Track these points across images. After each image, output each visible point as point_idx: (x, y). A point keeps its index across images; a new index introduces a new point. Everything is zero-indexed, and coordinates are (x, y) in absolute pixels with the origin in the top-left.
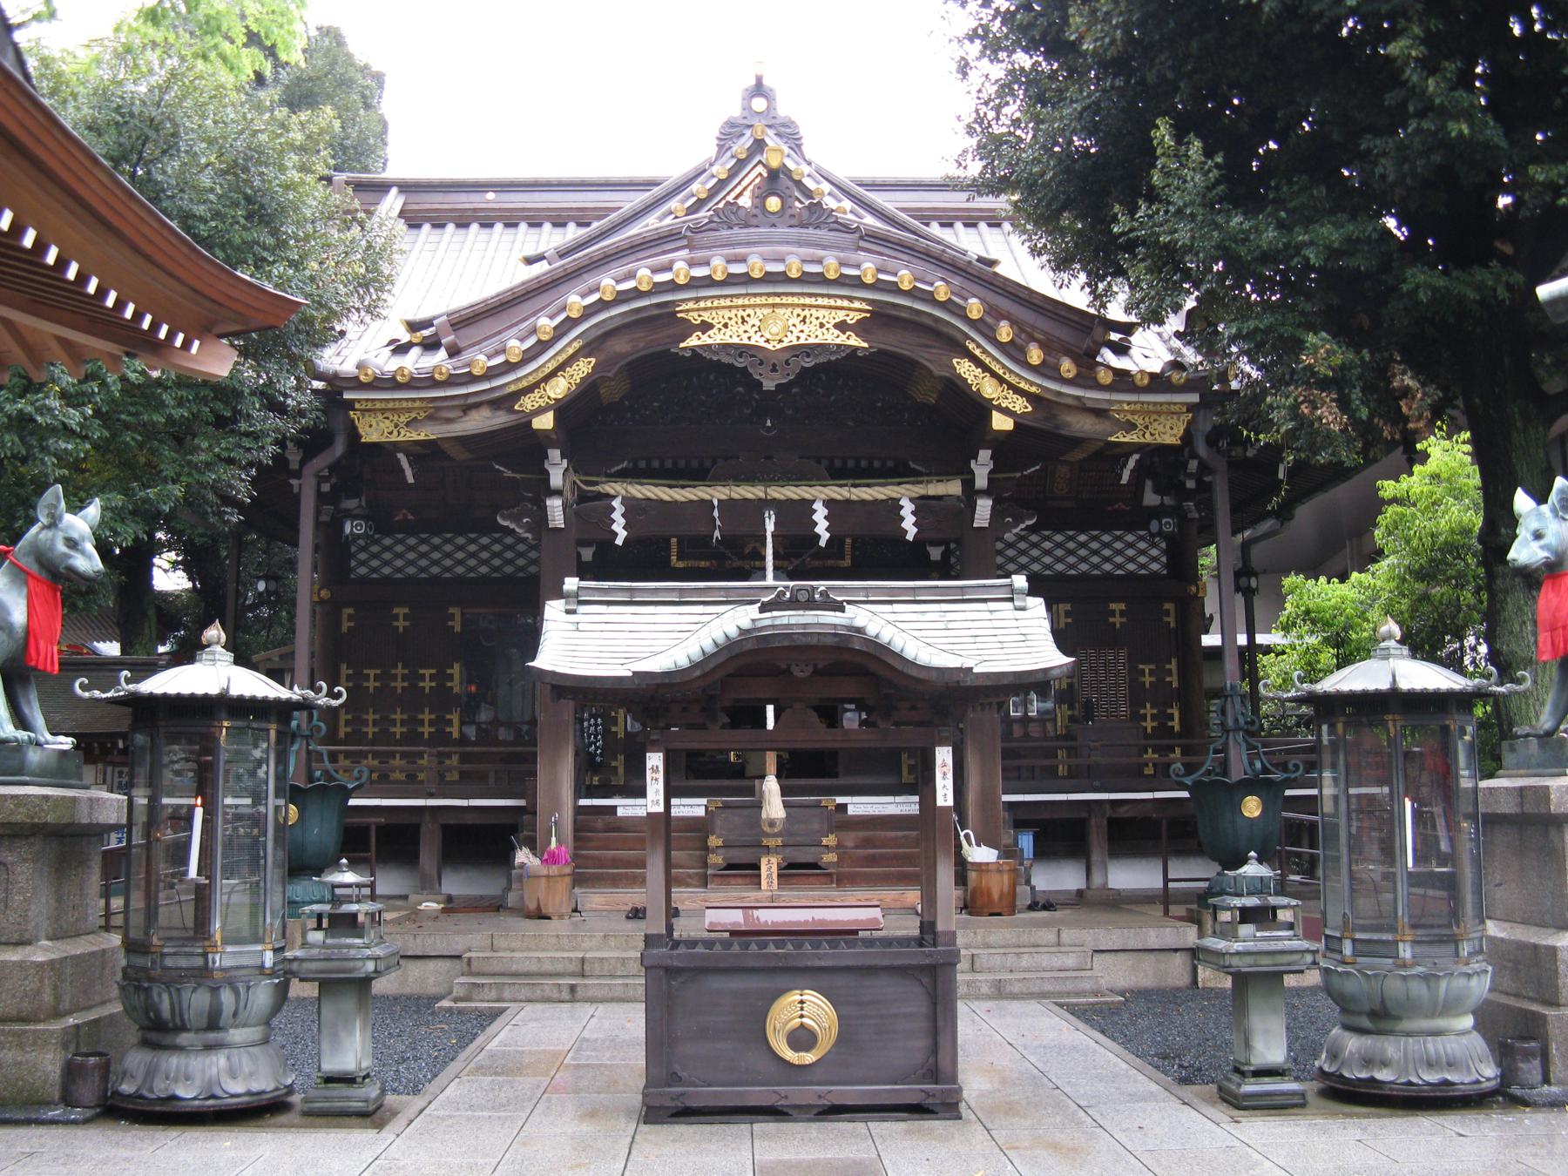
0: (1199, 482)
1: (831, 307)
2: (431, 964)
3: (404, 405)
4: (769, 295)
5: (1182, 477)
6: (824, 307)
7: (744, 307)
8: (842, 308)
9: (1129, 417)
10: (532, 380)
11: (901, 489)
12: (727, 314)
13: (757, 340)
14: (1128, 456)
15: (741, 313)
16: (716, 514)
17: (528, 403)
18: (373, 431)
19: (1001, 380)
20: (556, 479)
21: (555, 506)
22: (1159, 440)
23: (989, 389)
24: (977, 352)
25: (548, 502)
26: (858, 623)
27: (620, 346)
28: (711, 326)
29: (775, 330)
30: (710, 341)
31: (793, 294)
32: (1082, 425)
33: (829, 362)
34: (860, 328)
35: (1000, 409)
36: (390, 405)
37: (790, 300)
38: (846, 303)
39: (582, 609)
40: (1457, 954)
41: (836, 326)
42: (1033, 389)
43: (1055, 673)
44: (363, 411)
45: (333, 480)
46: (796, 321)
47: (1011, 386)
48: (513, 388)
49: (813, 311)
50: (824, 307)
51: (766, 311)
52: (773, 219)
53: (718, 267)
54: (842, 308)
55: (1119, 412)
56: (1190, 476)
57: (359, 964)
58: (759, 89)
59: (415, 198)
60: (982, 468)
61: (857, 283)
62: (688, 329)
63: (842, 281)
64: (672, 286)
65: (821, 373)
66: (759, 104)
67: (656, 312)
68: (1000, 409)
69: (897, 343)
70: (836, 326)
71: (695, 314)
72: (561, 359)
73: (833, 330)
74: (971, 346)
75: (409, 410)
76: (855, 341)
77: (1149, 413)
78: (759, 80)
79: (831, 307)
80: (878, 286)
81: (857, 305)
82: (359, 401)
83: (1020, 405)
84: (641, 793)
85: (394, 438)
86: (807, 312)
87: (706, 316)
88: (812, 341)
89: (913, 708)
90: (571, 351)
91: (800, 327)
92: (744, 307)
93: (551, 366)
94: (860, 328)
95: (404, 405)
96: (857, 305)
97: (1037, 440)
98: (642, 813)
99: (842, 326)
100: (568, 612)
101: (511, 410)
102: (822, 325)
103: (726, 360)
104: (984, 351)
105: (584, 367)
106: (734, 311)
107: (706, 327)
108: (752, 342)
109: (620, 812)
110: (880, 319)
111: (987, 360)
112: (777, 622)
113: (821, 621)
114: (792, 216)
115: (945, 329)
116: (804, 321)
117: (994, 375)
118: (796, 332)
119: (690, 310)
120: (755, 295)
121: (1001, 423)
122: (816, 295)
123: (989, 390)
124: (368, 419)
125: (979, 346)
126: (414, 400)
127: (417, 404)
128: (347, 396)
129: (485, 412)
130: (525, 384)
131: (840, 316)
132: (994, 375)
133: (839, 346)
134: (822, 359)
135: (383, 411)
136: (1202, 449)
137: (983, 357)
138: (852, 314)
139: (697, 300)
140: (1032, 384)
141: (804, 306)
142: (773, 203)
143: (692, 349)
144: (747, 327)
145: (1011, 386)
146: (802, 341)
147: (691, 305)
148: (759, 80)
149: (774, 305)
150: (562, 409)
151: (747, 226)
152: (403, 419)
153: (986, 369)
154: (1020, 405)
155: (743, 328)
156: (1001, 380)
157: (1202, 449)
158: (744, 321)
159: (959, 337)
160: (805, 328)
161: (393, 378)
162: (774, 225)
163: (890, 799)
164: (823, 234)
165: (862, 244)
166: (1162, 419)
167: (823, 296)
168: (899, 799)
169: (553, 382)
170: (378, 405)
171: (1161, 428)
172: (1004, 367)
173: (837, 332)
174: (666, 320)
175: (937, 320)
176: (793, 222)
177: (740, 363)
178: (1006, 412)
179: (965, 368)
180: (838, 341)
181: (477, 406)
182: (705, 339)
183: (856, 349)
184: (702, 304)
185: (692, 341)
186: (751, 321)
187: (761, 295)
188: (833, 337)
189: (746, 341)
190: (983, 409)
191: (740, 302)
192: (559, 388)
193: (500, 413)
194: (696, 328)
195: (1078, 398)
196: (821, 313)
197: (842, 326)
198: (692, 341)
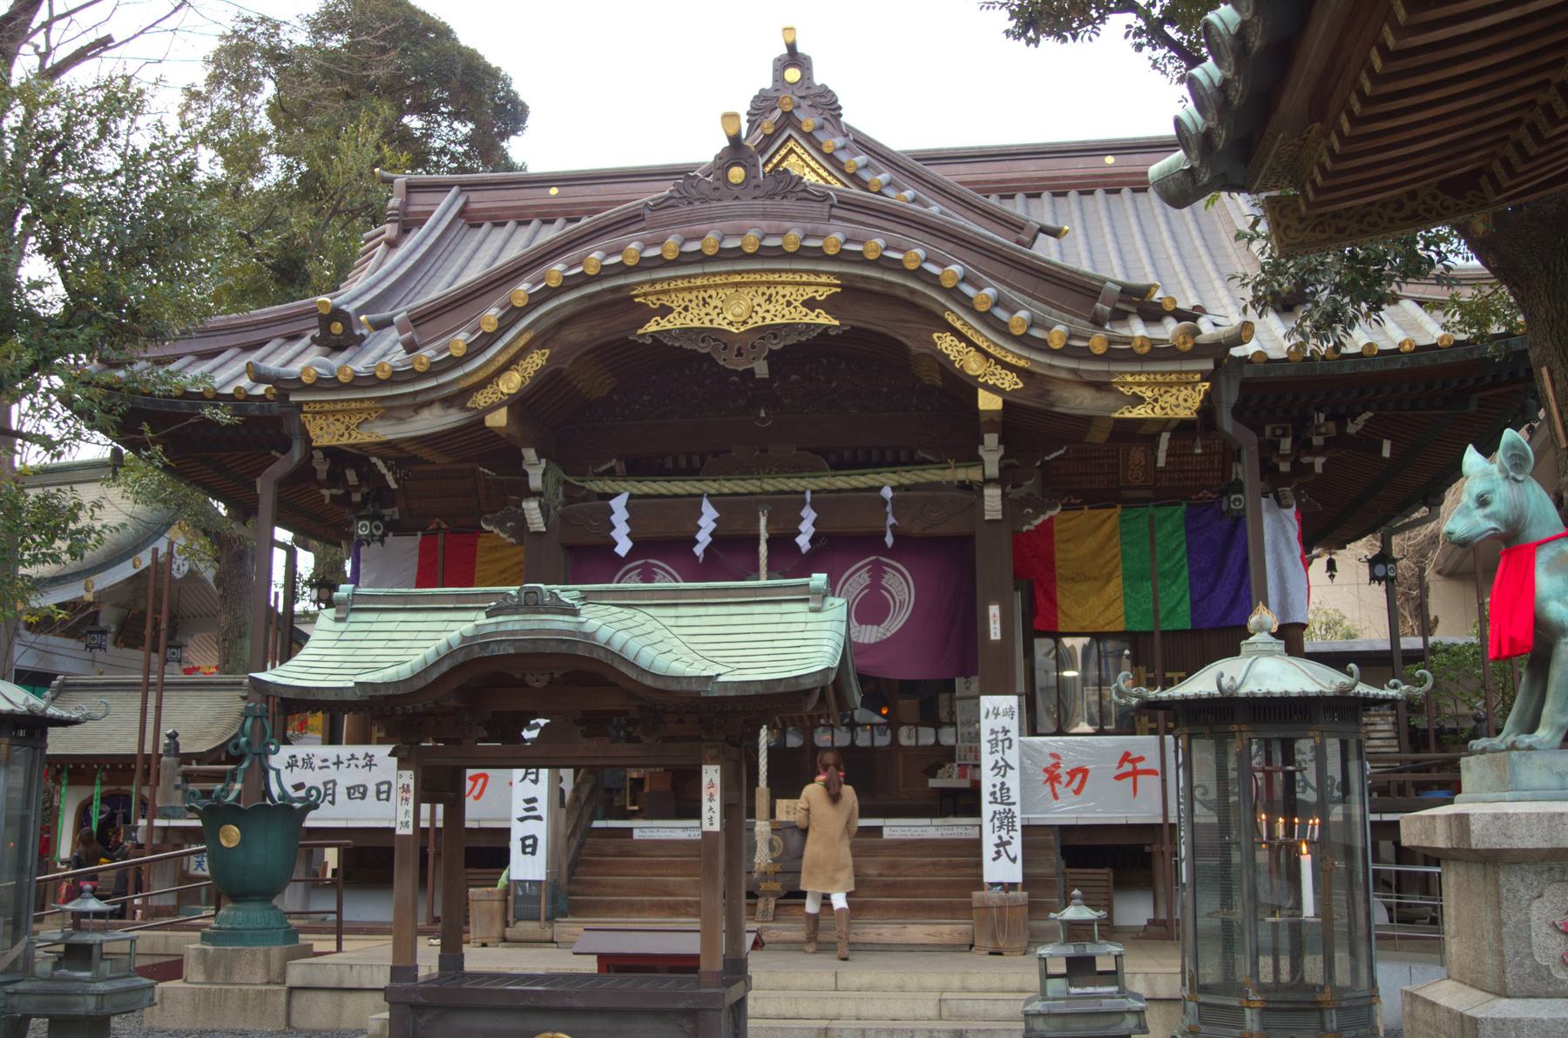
0: (1296, 464)
1: (798, 284)
2: (367, 995)
3: (353, 405)
4: (729, 273)
5: (1275, 460)
6: (790, 283)
7: (705, 288)
8: (810, 284)
9: (1136, 389)
10: (481, 375)
11: (804, 483)
12: (688, 296)
13: (720, 323)
14: (1158, 435)
15: (702, 294)
16: (889, 508)
17: (481, 399)
18: (325, 433)
19: (987, 355)
20: (535, 482)
21: (531, 508)
22: (1171, 414)
23: (973, 365)
24: (958, 325)
25: (524, 505)
26: (588, 628)
27: (576, 335)
28: (671, 310)
29: (738, 310)
30: (669, 326)
31: (754, 271)
32: (1081, 401)
33: (800, 343)
34: (830, 305)
35: (986, 386)
36: (339, 406)
37: (752, 277)
38: (812, 279)
39: (352, 617)
40: (1323, 1027)
41: (804, 304)
42: (1022, 363)
43: (808, 684)
44: (315, 413)
45: (365, 490)
46: (760, 300)
47: (998, 361)
48: (463, 384)
49: (779, 288)
50: (790, 283)
51: (729, 291)
52: (736, 191)
53: (672, 245)
54: (810, 284)
55: (1124, 384)
56: (1284, 457)
57: (81, 999)
58: (793, 57)
59: (474, 196)
60: (991, 451)
61: (819, 255)
62: (647, 314)
63: (802, 254)
64: (623, 269)
65: (796, 354)
66: (793, 75)
67: (610, 297)
68: (986, 386)
69: (873, 318)
70: (804, 304)
71: (653, 298)
72: (512, 351)
73: (801, 308)
74: (950, 318)
75: (360, 411)
76: (825, 319)
77: (1158, 384)
78: (792, 47)
79: (798, 284)
80: (842, 257)
81: (824, 279)
82: (307, 403)
83: (1009, 381)
84: (696, 813)
85: (344, 441)
86: (772, 290)
87: (665, 300)
88: (778, 321)
89: (681, 721)
90: (522, 343)
91: (766, 306)
92: (705, 288)
93: (502, 359)
94: (830, 305)
95: (353, 405)
96: (824, 279)
97: (1027, 424)
98: (696, 835)
99: (810, 304)
100: (337, 620)
101: (463, 408)
102: (789, 304)
103: (688, 346)
104: (965, 324)
105: (537, 360)
106: (695, 293)
107: (665, 311)
108: (715, 325)
109: (637, 835)
110: (850, 294)
111: (969, 334)
112: (502, 628)
113: (548, 626)
114: (757, 186)
115: (921, 301)
116: (769, 300)
117: (979, 349)
118: (761, 314)
119: (644, 290)
120: (714, 274)
121: (988, 402)
122: (780, 271)
123: (974, 366)
124: (321, 421)
125: (959, 318)
126: (362, 400)
127: (365, 405)
128: (292, 399)
129: (437, 410)
130: (475, 379)
131: (809, 292)
132: (979, 349)
133: (808, 325)
134: (792, 341)
135: (333, 413)
136: (1227, 423)
137: (964, 330)
138: (821, 290)
139: (653, 282)
140: (1020, 357)
141: (769, 284)
142: (737, 174)
143: (653, 335)
144: (709, 309)
145: (998, 361)
146: (768, 322)
147: (646, 288)
148: (792, 47)
149: (737, 285)
150: (519, 404)
151: (704, 200)
152: (354, 421)
153: (970, 343)
154: (1009, 381)
155: (704, 310)
156: (987, 355)
157: (1227, 423)
158: (705, 303)
159: (938, 310)
160: (771, 307)
161: (299, 379)
162: (737, 198)
163: (927, 821)
164: (789, 204)
165: (835, 211)
166: (1174, 390)
167: (786, 271)
168: (936, 821)
169: (506, 376)
170: (327, 407)
171: (1172, 400)
172: (988, 340)
173: (805, 310)
174: (622, 305)
175: (912, 291)
176: (757, 193)
177: (703, 349)
178: (994, 389)
179: (946, 343)
180: (806, 320)
181: (429, 404)
182: (665, 324)
183: (830, 327)
184: (658, 287)
185: (652, 327)
186: (713, 303)
187: (720, 274)
189: (708, 325)
190: (966, 388)
191: (699, 282)
192: (512, 383)
193: (452, 411)
194: (655, 313)
195: (1074, 371)
196: (788, 290)
197: (810, 304)
198: (652, 327)
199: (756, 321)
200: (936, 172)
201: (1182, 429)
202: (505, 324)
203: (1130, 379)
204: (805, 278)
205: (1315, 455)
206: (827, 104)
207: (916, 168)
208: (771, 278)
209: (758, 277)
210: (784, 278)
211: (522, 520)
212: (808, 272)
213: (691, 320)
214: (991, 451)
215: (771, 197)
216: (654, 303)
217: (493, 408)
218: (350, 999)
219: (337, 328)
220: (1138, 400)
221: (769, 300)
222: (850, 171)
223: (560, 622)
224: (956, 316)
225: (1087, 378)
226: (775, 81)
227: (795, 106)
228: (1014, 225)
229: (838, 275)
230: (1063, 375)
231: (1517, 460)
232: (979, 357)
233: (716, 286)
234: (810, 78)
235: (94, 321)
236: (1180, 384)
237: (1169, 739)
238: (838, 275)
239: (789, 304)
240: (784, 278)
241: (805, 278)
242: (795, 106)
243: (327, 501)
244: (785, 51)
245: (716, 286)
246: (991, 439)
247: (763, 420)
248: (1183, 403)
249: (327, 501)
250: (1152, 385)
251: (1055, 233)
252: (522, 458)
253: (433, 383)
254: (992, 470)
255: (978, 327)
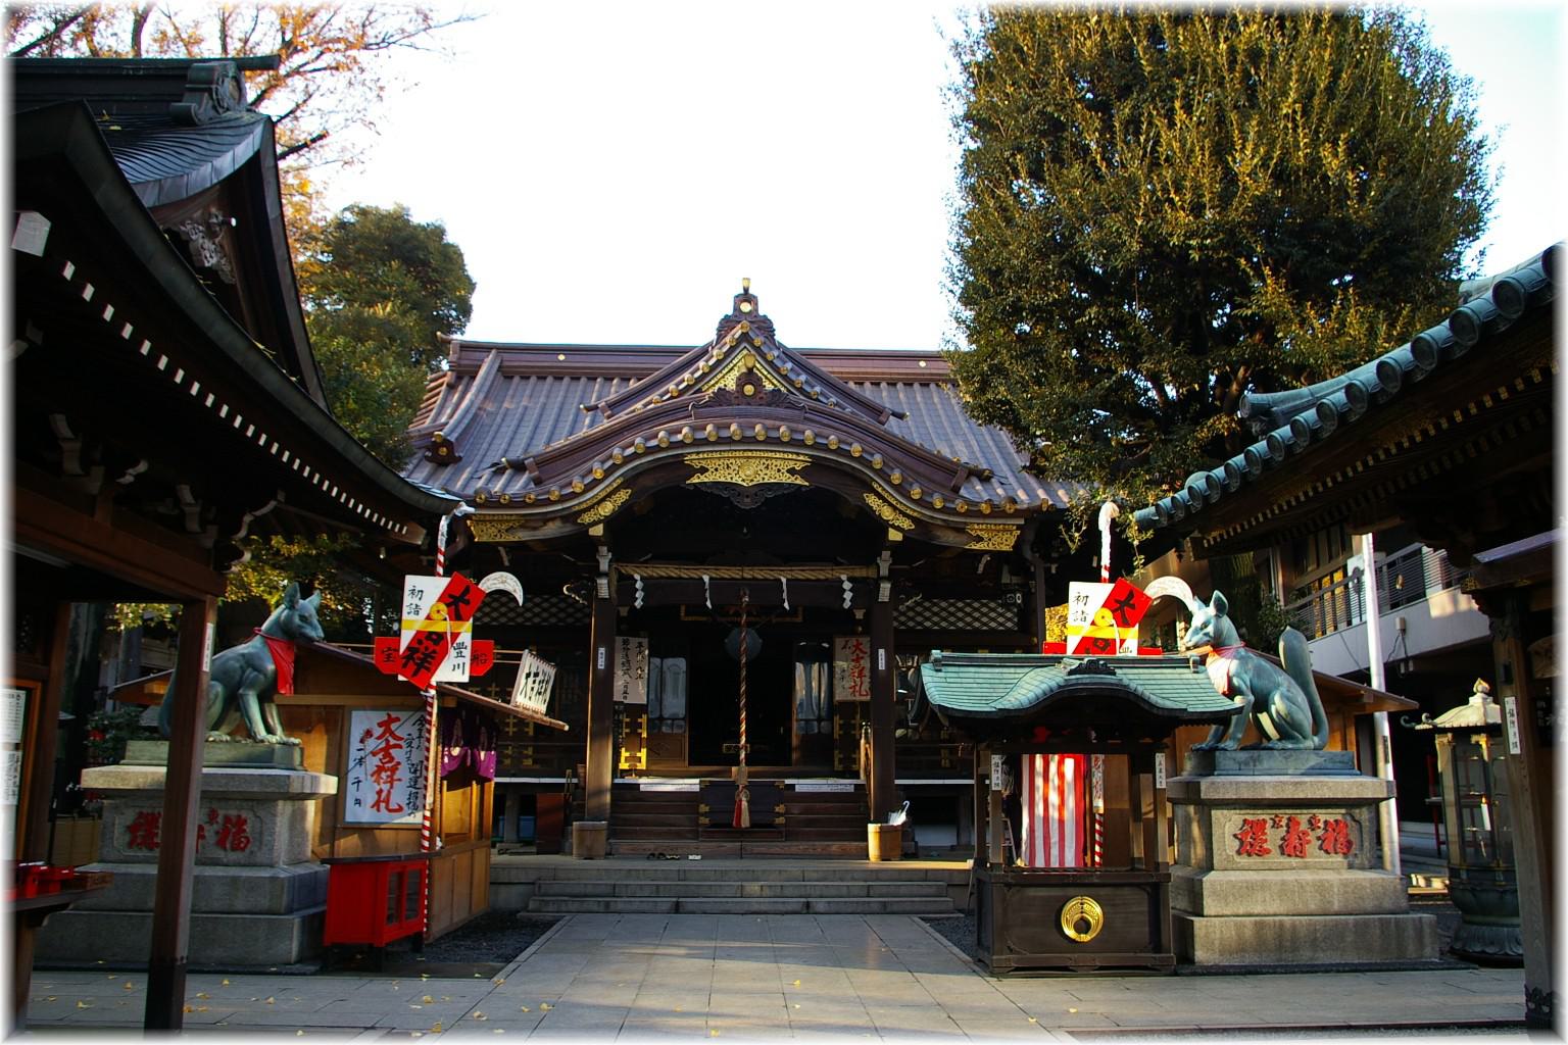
9: (979, 533)
10: (589, 503)
17: (587, 518)
20: (604, 566)
23: (887, 513)
24: (880, 490)
27: (647, 482)
28: (707, 470)
29: (748, 473)
30: (706, 480)
32: (949, 538)
34: (803, 473)
35: (893, 526)
38: (794, 457)
41: (788, 471)
42: (915, 514)
47: (901, 512)
48: (577, 508)
58: (746, 296)
59: (506, 356)
62: (693, 471)
65: (774, 498)
66: (746, 307)
68: (893, 526)
69: (827, 482)
70: (788, 471)
76: (799, 481)
78: (746, 290)
81: (801, 458)
83: (906, 524)
87: (704, 463)
91: (765, 471)
94: (803, 473)
96: (801, 458)
99: (792, 471)
102: (779, 471)
103: (716, 492)
104: (884, 489)
105: (623, 496)
107: (703, 470)
110: (817, 467)
115: (858, 474)
116: (767, 468)
119: (692, 458)
121: (894, 536)
130: (585, 506)
131: (791, 464)
132: (890, 505)
135: (490, 522)
137: (883, 493)
139: (698, 453)
141: (767, 458)
144: (730, 471)
145: (901, 512)
147: (694, 456)
148: (746, 290)
149: (749, 457)
150: (608, 522)
153: (885, 500)
154: (906, 524)
156: (895, 508)
164: (781, 411)
169: (603, 505)
177: (725, 494)
178: (898, 528)
179: (872, 501)
180: (789, 481)
181: (553, 519)
182: (704, 478)
183: (801, 486)
184: (701, 456)
185: (695, 480)
188: (786, 479)
192: (607, 509)
196: (778, 462)
197: (792, 471)
199: (758, 480)
200: (815, 363)
201: (998, 556)
202: (608, 473)
203: (976, 527)
204: (790, 456)
205: (1052, 563)
206: (765, 327)
207: (802, 360)
208: (770, 455)
209: (762, 454)
210: (778, 456)
211: (595, 588)
212: (792, 453)
213: (721, 477)
214: (884, 564)
215: (769, 405)
216: (697, 465)
217: (595, 523)
218: (503, 888)
219: (443, 451)
220: (979, 539)
221: (767, 468)
222: (799, 386)
223: (1108, 678)
224: (879, 485)
225: (952, 525)
226: (735, 310)
227: (748, 326)
228: (876, 411)
229: (811, 456)
230: (939, 522)
231: (1220, 607)
232: (890, 510)
233: (735, 458)
234: (757, 310)
235: (1469, 837)
236: (1004, 530)
237: (1098, 763)
238: (811, 456)
239: (779, 471)
240: (778, 456)
241: (790, 456)
242: (748, 326)
243: (425, 563)
244: (742, 292)
245: (735, 458)
246: (886, 554)
247: (746, 535)
248: (1005, 542)
249: (425, 563)
250: (986, 530)
251: (901, 416)
252: (597, 551)
253: (559, 507)
254: (884, 571)
255: (892, 492)
